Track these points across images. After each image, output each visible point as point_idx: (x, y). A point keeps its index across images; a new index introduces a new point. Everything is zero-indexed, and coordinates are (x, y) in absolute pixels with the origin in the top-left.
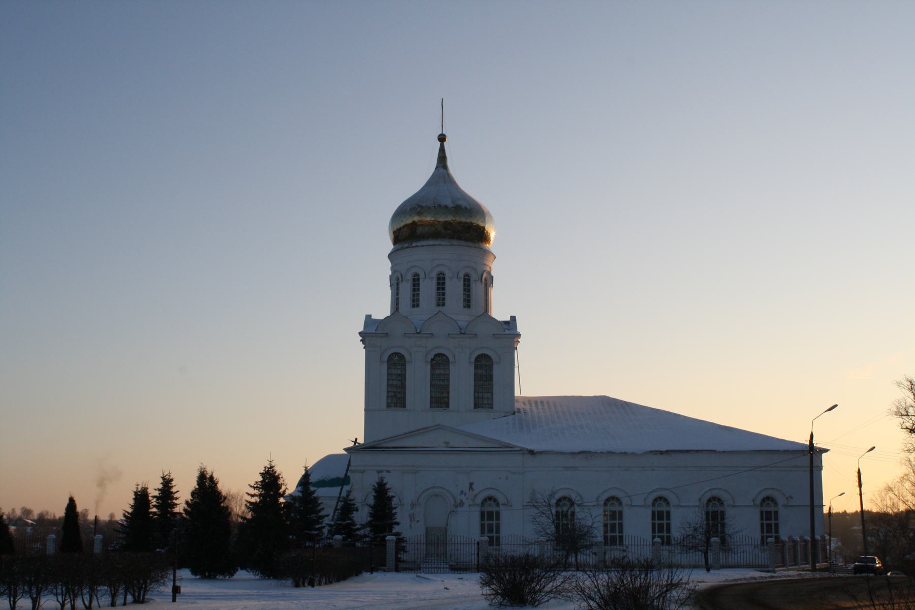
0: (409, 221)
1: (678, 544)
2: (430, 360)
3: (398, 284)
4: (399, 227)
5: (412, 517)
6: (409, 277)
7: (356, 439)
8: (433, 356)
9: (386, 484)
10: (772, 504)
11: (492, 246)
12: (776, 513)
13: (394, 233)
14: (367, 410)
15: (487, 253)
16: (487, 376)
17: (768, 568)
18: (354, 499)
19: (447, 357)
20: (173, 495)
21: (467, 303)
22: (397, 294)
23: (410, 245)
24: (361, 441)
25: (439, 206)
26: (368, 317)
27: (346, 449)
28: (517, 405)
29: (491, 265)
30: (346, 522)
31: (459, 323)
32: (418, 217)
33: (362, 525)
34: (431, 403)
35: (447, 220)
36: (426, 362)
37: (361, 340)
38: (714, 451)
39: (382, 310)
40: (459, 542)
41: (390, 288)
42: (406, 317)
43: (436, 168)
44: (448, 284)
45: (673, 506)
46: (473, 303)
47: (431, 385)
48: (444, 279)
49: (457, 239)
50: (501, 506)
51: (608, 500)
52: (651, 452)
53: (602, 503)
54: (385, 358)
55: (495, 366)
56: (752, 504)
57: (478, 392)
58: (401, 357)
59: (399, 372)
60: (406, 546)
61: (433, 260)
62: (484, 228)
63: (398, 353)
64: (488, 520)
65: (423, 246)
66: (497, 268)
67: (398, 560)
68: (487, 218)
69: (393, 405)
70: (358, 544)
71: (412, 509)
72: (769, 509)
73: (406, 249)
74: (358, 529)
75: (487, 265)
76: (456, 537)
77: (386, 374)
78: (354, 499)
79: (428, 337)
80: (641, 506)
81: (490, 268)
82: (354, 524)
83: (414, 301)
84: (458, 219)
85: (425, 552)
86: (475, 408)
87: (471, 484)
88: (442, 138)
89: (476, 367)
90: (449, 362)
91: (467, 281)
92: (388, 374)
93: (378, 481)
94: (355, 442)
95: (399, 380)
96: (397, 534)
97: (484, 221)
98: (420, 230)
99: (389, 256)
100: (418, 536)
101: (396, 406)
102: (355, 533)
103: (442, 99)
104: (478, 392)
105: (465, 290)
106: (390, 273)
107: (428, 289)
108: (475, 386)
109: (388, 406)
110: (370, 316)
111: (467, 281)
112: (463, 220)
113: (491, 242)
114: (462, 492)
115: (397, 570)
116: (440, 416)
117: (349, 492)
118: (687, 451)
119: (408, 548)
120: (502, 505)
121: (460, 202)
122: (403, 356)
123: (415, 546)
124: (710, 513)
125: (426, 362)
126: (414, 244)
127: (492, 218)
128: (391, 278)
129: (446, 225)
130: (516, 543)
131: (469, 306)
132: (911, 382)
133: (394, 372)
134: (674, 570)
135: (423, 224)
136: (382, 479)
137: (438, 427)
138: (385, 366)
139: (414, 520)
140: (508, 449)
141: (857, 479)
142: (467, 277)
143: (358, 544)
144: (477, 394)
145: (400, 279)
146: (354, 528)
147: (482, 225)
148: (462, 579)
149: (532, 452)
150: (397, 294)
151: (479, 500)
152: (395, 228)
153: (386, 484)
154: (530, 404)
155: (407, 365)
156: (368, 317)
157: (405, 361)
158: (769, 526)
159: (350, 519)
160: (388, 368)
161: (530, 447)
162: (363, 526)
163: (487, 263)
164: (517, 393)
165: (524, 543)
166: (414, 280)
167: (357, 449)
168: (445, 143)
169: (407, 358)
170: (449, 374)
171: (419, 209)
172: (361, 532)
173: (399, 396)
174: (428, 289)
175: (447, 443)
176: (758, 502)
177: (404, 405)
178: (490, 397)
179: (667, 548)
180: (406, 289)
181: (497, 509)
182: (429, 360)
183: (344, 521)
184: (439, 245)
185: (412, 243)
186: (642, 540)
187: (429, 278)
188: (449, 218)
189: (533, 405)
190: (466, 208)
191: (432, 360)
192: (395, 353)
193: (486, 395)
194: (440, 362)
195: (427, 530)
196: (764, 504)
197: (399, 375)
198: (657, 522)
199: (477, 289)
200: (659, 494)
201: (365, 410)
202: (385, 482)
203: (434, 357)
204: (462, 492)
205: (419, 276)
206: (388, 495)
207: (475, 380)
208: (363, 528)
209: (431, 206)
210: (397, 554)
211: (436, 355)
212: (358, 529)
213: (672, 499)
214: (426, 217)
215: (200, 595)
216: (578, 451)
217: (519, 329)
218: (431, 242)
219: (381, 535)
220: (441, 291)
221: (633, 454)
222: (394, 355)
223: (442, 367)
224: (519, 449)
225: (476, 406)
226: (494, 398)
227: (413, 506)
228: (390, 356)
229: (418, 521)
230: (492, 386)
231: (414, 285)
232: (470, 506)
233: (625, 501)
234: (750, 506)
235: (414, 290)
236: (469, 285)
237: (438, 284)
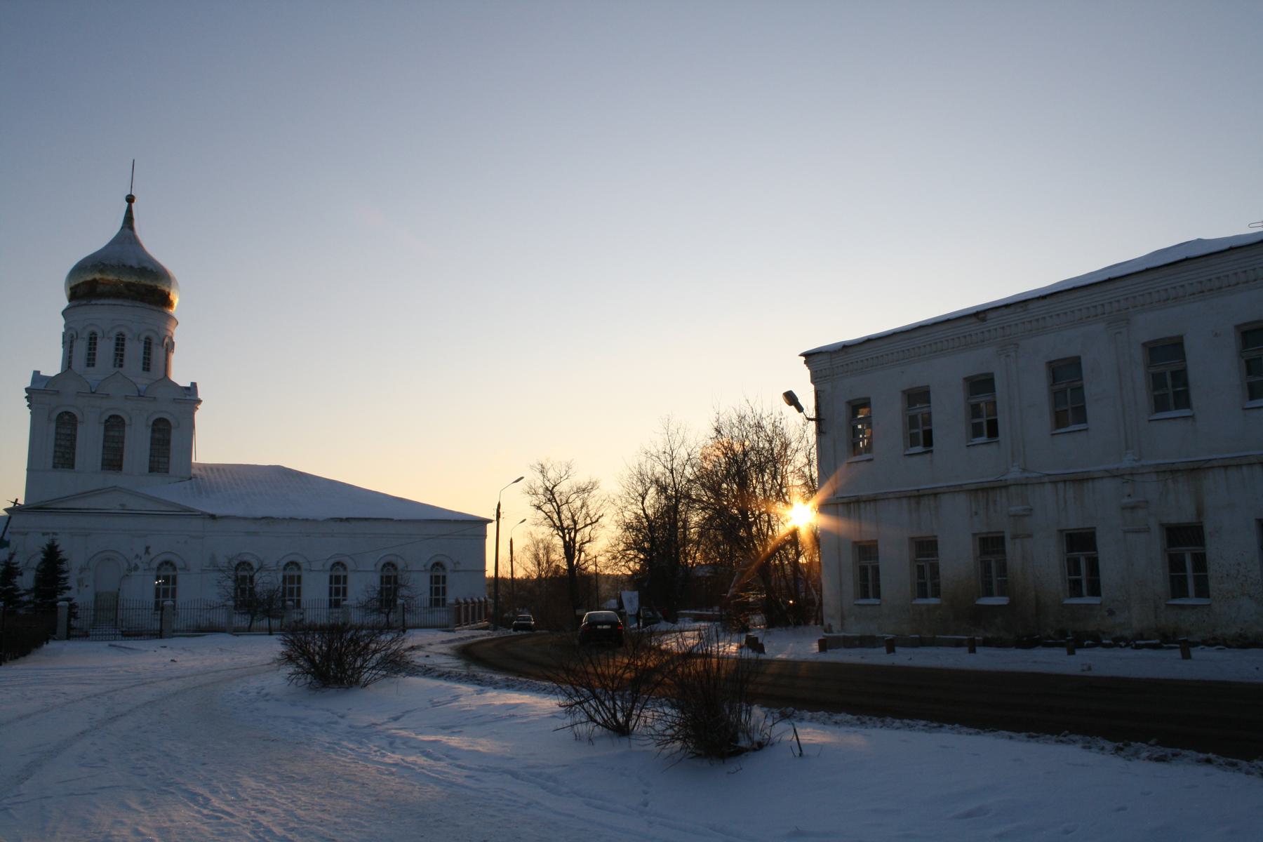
0: (89, 278)
1: (363, 606)
3: (72, 342)
4: (76, 283)
5: (80, 582)
6: (86, 335)
7: (17, 500)
9: (57, 546)
10: (440, 569)
11: (173, 312)
12: (444, 577)
13: (71, 289)
14: (30, 470)
15: (170, 317)
17: (448, 627)
18: (18, 563)
21: (147, 366)
22: (71, 352)
24: (22, 501)
25: (124, 266)
26: (36, 373)
27: (6, 510)
28: (194, 471)
29: (172, 330)
30: (8, 587)
31: (138, 386)
33: (26, 590)
34: (103, 465)
35: (130, 280)
37: (26, 397)
38: (392, 520)
39: (52, 367)
40: (134, 607)
41: (62, 345)
42: (80, 376)
43: (122, 228)
44: (128, 346)
45: (179, 569)
47: (104, 447)
50: (178, 570)
51: (288, 565)
52: (332, 519)
53: (282, 567)
54: (54, 416)
55: (173, 431)
56: (423, 569)
57: (154, 456)
58: (72, 416)
59: (69, 432)
60: (77, 612)
62: (169, 294)
66: (179, 335)
67: (70, 628)
68: (173, 283)
70: (22, 611)
71: (80, 573)
72: (338, 574)
74: (22, 595)
78: (18, 563)
80: (319, 571)
81: (172, 333)
82: (16, 589)
83: (89, 360)
84: (143, 282)
85: (92, 618)
86: (150, 472)
87: (148, 548)
88: (130, 199)
89: (153, 431)
90: (125, 424)
91: (148, 344)
93: (48, 543)
94: (15, 503)
95: (68, 440)
96: (68, 600)
97: (169, 286)
98: (100, 288)
100: (312, 601)
101: (63, 467)
102: (17, 599)
103: (134, 161)
104: (154, 456)
105: (145, 353)
106: (63, 330)
107: (105, 349)
108: (151, 450)
109: (55, 466)
111: (148, 344)
112: (148, 282)
113: (175, 308)
114: (137, 556)
115: (69, 637)
116: (113, 479)
117: (12, 555)
118: (366, 519)
119: (79, 614)
120: (451, 571)
121: (146, 265)
122: (74, 415)
126: (93, 302)
127: (177, 284)
128: (64, 335)
129: (128, 285)
130: (322, 607)
132: (542, 465)
134: (185, 629)
136: (53, 541)
137: (115, 489)
138: (53, 425)
139: (83, 585)
140: (188, 513)
141: (509, 547)
143: (22, 611)
144: (152, 458)
145: (75, 337)
146: (16, 593)
147: (167, 290)
148: (165, 647)
149: (213, 517)
150: (71, 352)
151: (155, 564)
152: (73, 284)
153: (57, 546)
154: (206, 471)
155: (79, 425)
156: (36, 373)
157: (76, 421)
158: (337, 590)
159: (12, 584)
160: (57, 428)
161: (211, 512)
162: (28, 592)
164: (193, 461)
165: (205, 607)
166: (91, 339)
167: (15, 510)
169: (79, 417)
172: (26, 598)
173: (67, 456)
174: (105, 349)
175: (123, 505)
176: (429, 567)
177: (72, 466)
179: (337, 610)
180: (81, 348)
181: (174, 573)
182: (103, 421)
183: (6, 586)
184: (122, 305)
188: (134, 279)
189: (210, 471)
190: (152, 271)
191: (106, 421)
192: (65, 412)
194: (114, 424)
195: (97, 595)
196: (434, 569)
197: (69, 435)
199: (157, 352)
200: (337, 559)
201: (28, 470)
202: (56, 544)
203: (109, 419)
204: (137, 556)
206: (59, 558)
207: (152, 444)
208: (27, 594)
210: (69, 621)
211: (111, 417)
212: (22, 595)
213: (350, 564)
216: (260, 517)
217: (200, 396)
219: (50, 601)
220: (120, 352)
221: (314, 520)
224: (200, 513)
225: (151, 470)
226: (171, 461)
227: (82, 570)
229: (87, 586)
231: (90, 344)
232: (145, 570)
233: (304, 566)
234: (422, 571)
235: (90, 349)
236: (150, 349)
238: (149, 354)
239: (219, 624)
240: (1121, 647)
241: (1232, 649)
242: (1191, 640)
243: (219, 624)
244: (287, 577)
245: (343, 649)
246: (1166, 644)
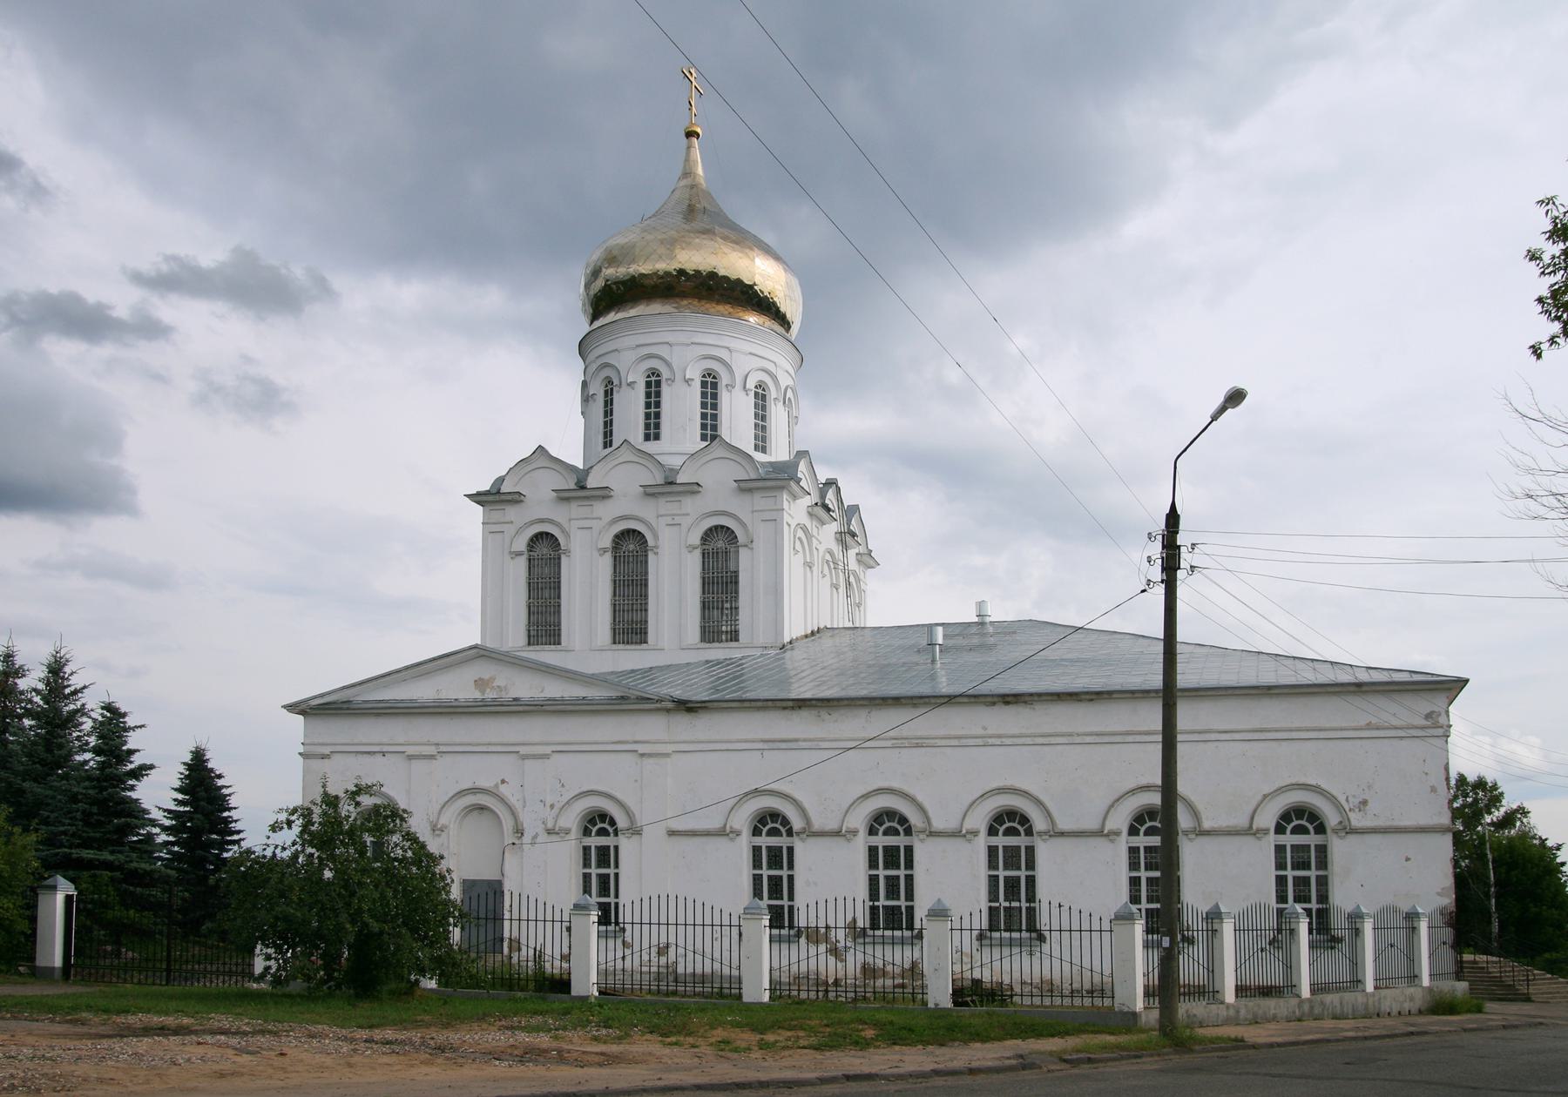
2: (697, 542)
64: (1006, 868)
76: (1055, 911)
123: (155, 954)
124: (1289, 849)
142: (709, 380)
186: (1085, 916)
187: (628, 385)
198: (1002, 873)
205: (658, 376)
215: (1139, 1057)
233: (1039, 823)
236: (715, 396)
238: (715, 406)
239: (1374, 1006)
240: (21, 974)
241: (1010, 706)
242: (1180, 574)
243: (1374, 1006)
244: (612, 835)
245: (285, 1034)
246: (1156, 827)
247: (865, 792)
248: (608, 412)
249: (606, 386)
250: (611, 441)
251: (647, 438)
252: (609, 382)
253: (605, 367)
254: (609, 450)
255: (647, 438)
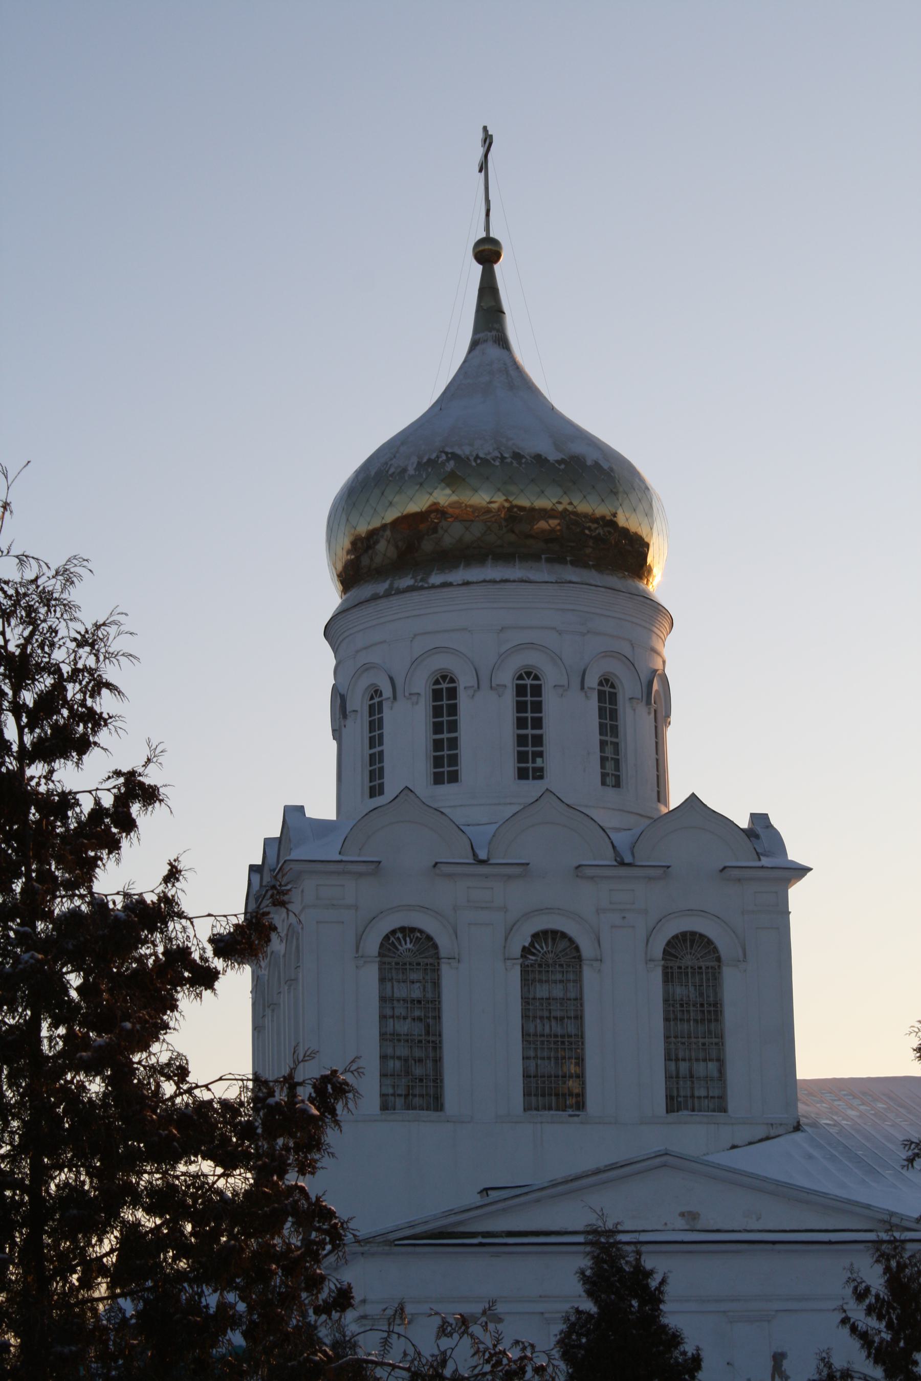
2: (518, 952)
6: (422, 684)
8: (529, 939)
16: (702, 1005)
19: (571, 940)
20: (448, 1372)
23: (422, 580)
25: (517, 456)
32: (448, 491)
34: (527, 1094)
36: (506, 959)
43: (474, 344)
46: (628, 771)
47: (525, 1035)
48: (537, 690)
49: (573, 563)
54: (372, 945)
57: (677, 1060)
58: (426, 942)
59: (416, 992)
61: (503, 629)
63: (413, 930)
65: (467, 583)
69: (400, 1101)
73: (407, 595)
75: (659, 654)
77: (377, 998)
79: (509, 877)
83: (438, 762)
90: (579, 958)
92: (383, 999)
95: (420, 1019)
99: (328, 632)
101: (409, 1107)
109: (384, 1107)
110: (301, 809)
122: (429, 938)
125: (506, 959)
131: (617, 784)
133: (401, 991)
135: (469, 515)
138: (372, 972)
155: (444, 968)
160: (382, 980)
163: (658, 646)
168: (497, 267)
169: (443, 942)
170: (579, 1000)
171: (451, 464)
173: (418, 1071)
177: (436, 1103)
178: (715, 1074)
185: (429, 574)
190: (597, 465)
191: (526, 951)
192: (403, 929)
193: (700, 1069)
203: (532, 944)
207: (667, 1020)
209: (488, 457)
211: (536, 936)
214: (476, 490)
218: (492, 572)
222: (400, 935)
223: (559, 976)
225: (674, 1104)
228: (387, 937)
230: (722, 1037)
235: (437, 728)
236: (614, 715)
237: (521, 707)
247: (379, 1084)
248: (376, 740)
249: (372, 698)
250: (381, 786)
251: (438, 779)
252: (376, 691)
253: (367, 669)
254: (379, 801)
255: (438, 779)
